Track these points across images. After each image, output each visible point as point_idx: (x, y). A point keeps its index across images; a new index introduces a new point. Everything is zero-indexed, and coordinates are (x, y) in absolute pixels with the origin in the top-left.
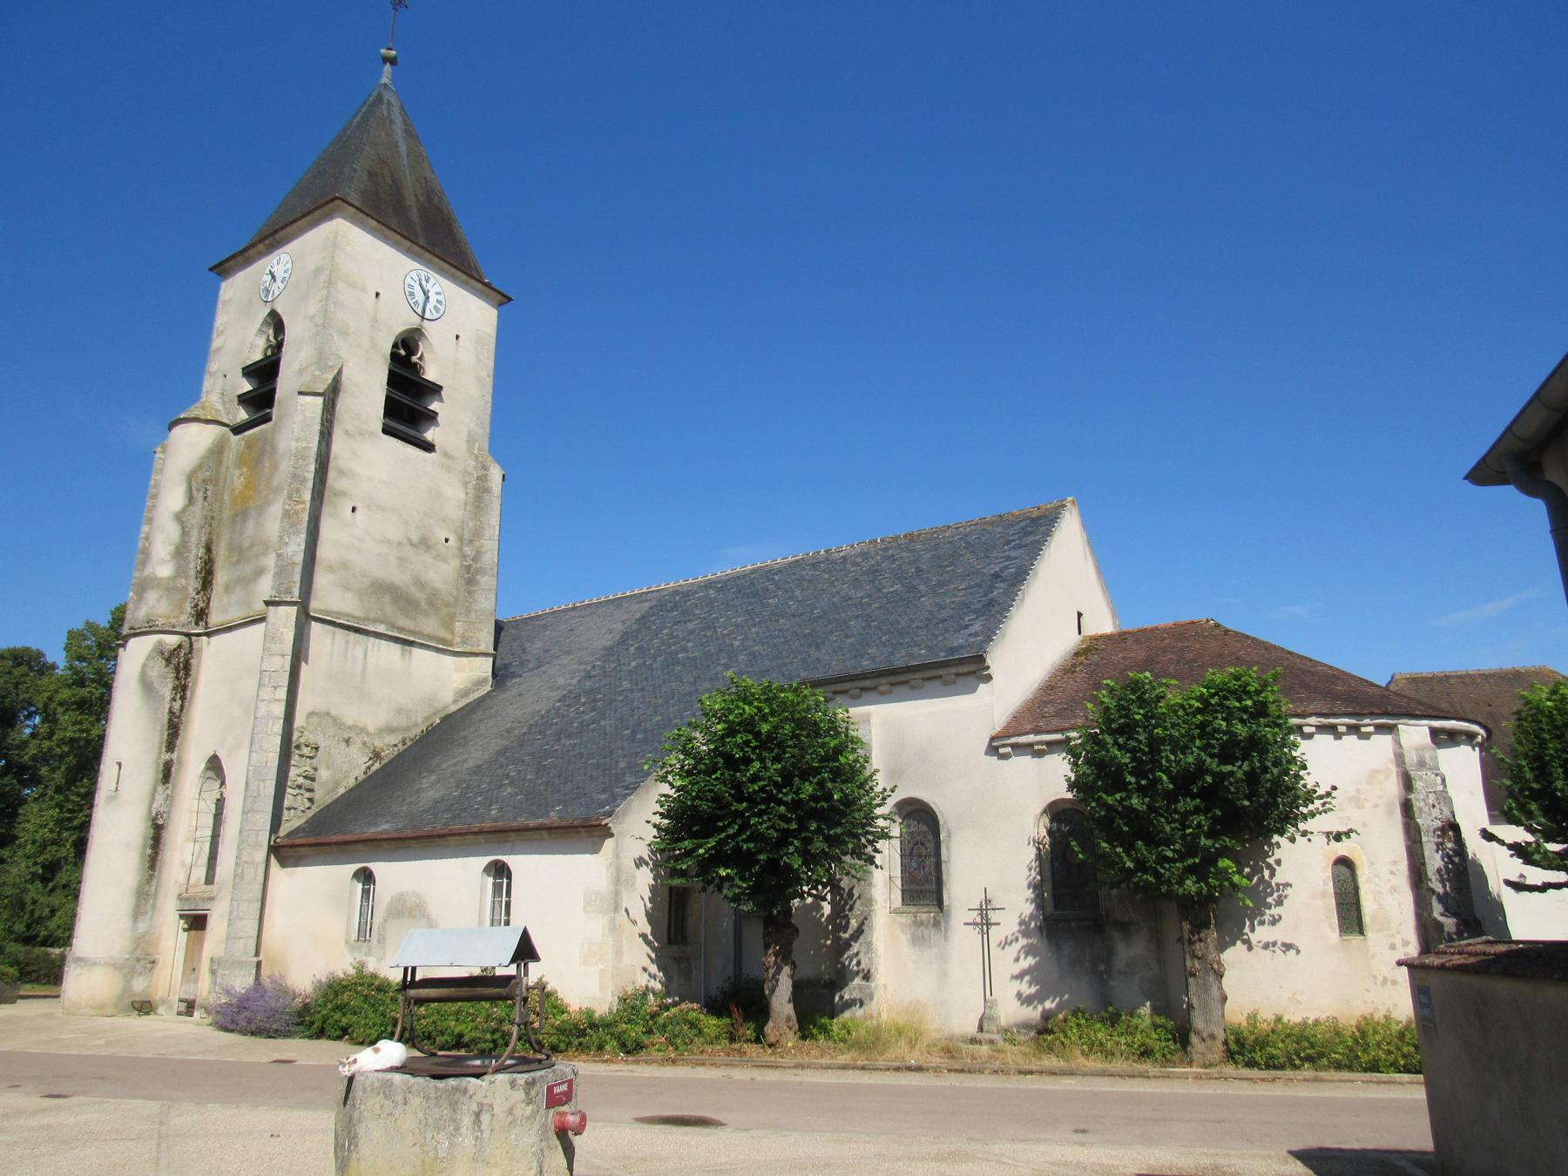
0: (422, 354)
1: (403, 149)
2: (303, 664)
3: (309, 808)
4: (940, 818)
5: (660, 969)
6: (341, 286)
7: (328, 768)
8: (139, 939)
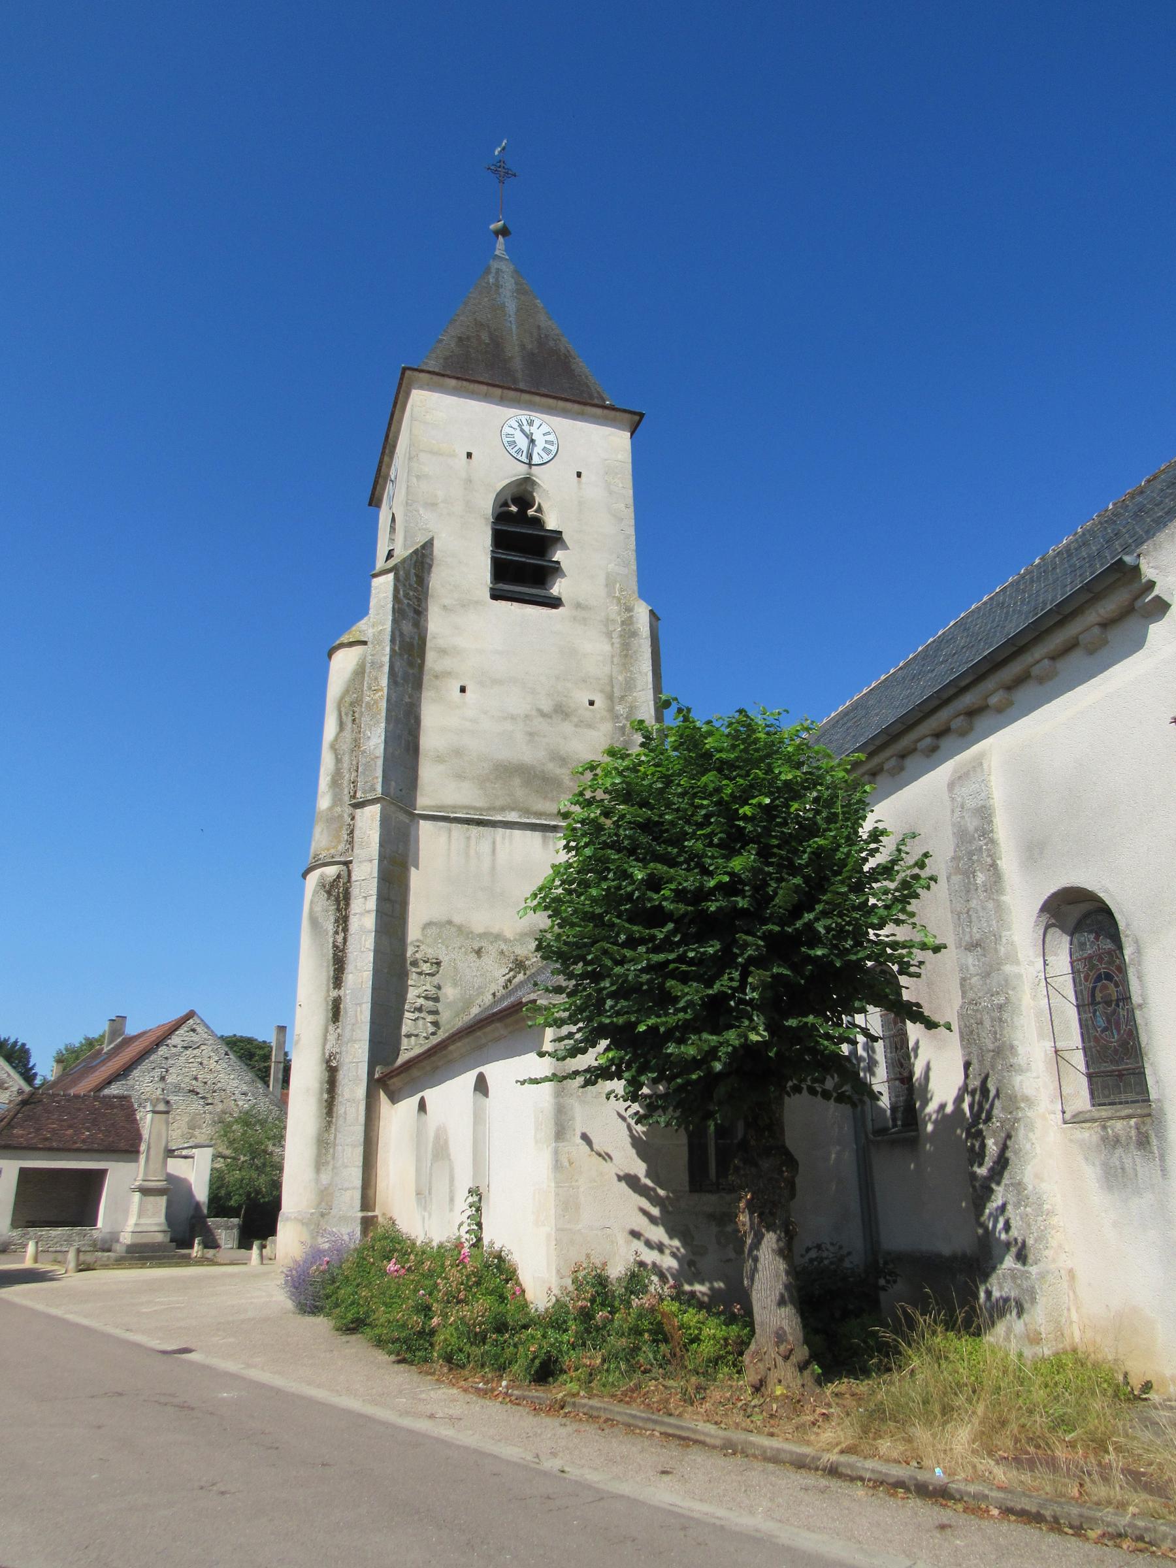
0: (539, 504)
1: (511, 307)
2: (413, 870)
3: (433, 1034)
4: (1118, 916)
5: (671, 1234)
6: (423, 457)
7: (455, 985)
8: (322, 1191)
